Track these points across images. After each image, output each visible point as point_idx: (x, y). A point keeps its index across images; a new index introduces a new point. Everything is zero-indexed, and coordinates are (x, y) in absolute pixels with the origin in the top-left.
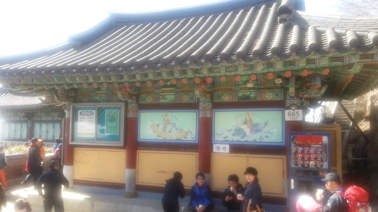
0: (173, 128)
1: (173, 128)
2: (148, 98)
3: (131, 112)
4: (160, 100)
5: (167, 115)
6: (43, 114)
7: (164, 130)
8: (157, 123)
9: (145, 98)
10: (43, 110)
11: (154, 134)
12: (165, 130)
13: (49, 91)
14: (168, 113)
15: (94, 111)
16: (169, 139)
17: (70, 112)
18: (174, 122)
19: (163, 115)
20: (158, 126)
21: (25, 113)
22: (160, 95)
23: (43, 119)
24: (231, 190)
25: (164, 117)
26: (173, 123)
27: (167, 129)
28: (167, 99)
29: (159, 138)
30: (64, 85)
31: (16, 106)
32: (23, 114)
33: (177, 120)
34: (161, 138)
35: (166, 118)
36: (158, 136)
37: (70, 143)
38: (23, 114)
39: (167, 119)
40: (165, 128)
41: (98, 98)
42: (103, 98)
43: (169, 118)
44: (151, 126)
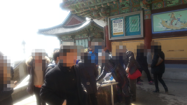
0: (178, 22)
1: (178, 22)
2: (158, 5)
3: (147, 16)
4: (167, 5)
5: (173, 14)
6: (79, 36)
7: (171, 24)
8: (166, 20)
9: (156, 5)
10: (78, 34)
11: (164, 27)
12: (172, 24)
13: (96, 11)
14: (174, 13)
15: (122, 19)
16: (175, 29)
17: (108, 22)
18: (179, 18)
19: (170, 15)
20: (166, 22)
21: (71, 36)
22: (167, 2)
23: (79, 38)
24: (12, 94)
25: (171, 15)
26: (177, 18)
27: (174, 23)
28: (172, 3)
29: (167, 30)
30: (102, 5)
31: (67, 32)
32: (70, 36)
33: (181, 16)
34: (169, 30)
35: (172, 16)
36: (167, 28)
37: (109, 39)
38: (70, 36)
39: (173, 17)
40: (172, 22)
41: (124, 11)
42: (127, 11)
43: (174, 16)
44: (161, 23)
